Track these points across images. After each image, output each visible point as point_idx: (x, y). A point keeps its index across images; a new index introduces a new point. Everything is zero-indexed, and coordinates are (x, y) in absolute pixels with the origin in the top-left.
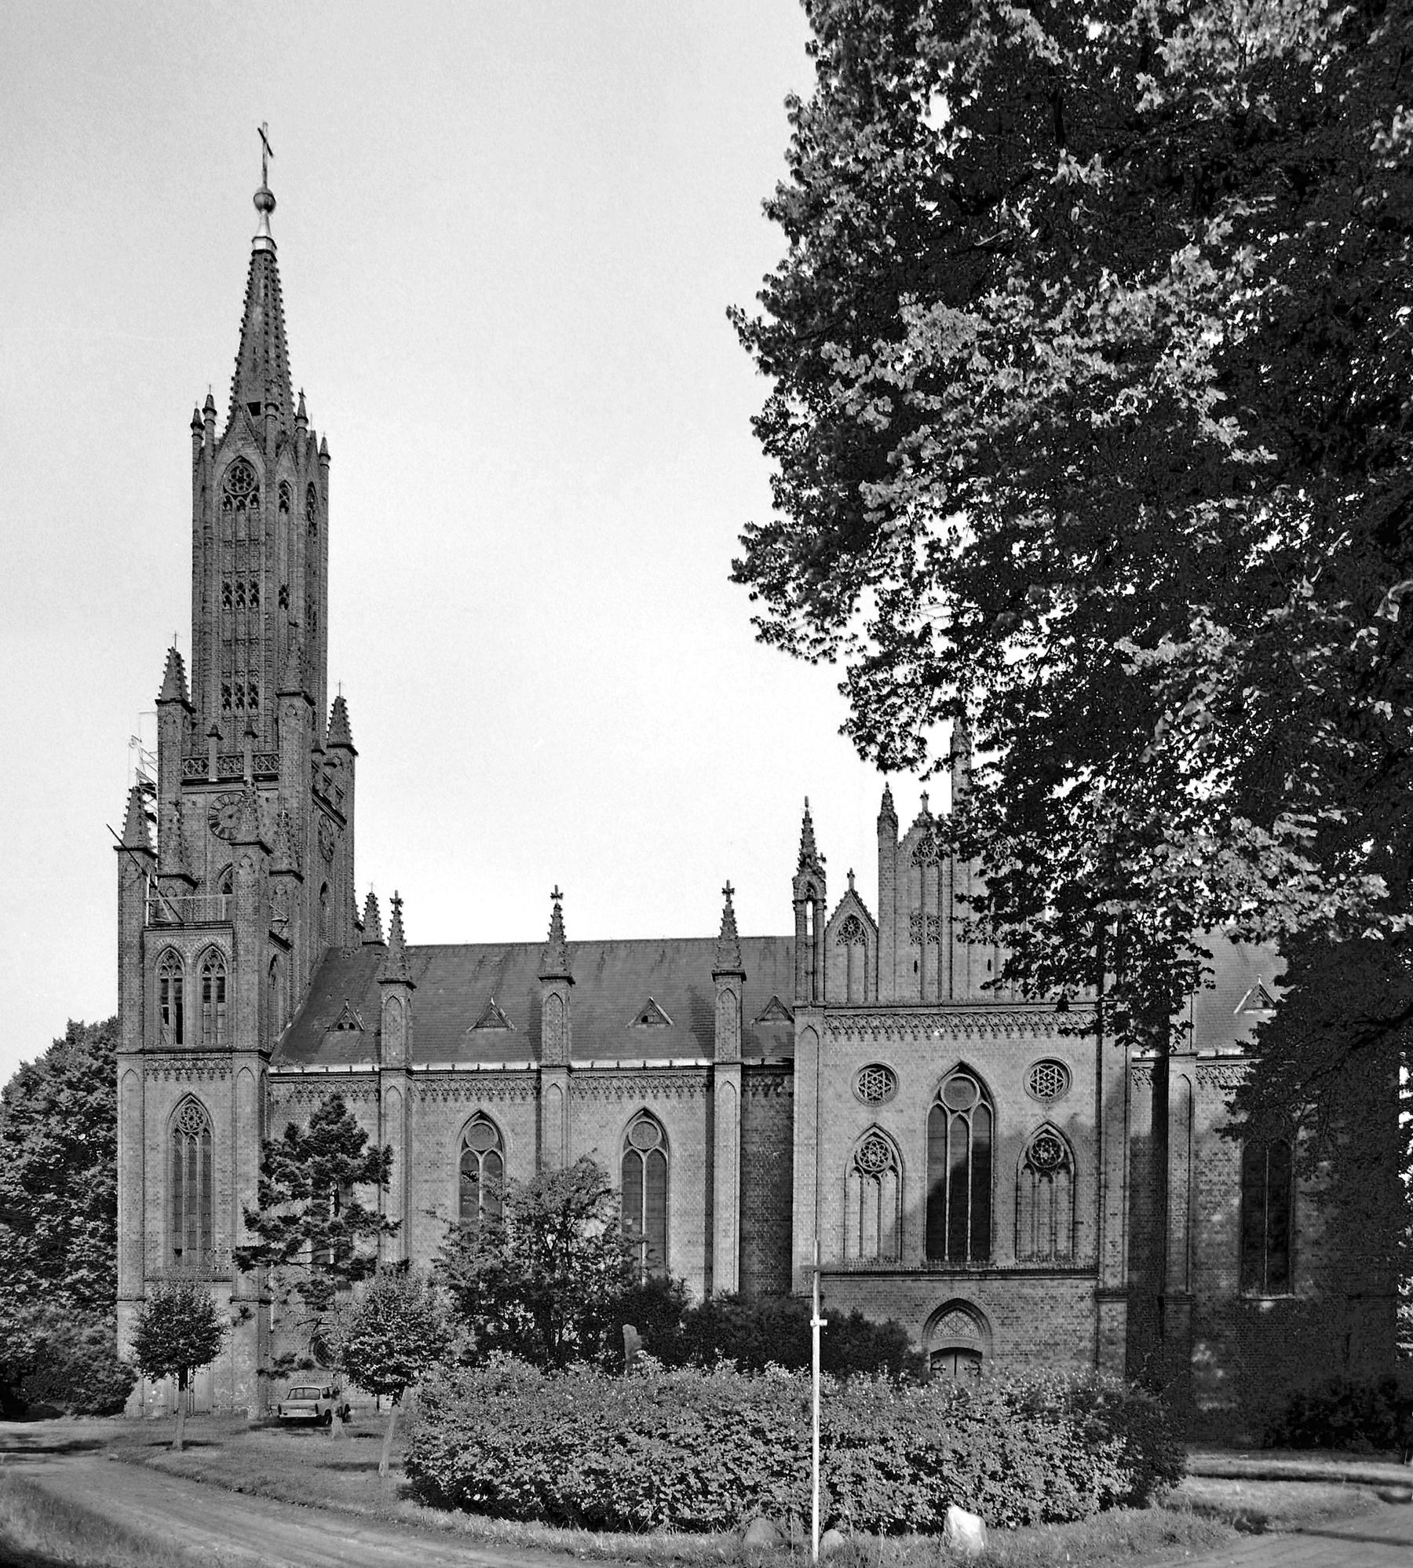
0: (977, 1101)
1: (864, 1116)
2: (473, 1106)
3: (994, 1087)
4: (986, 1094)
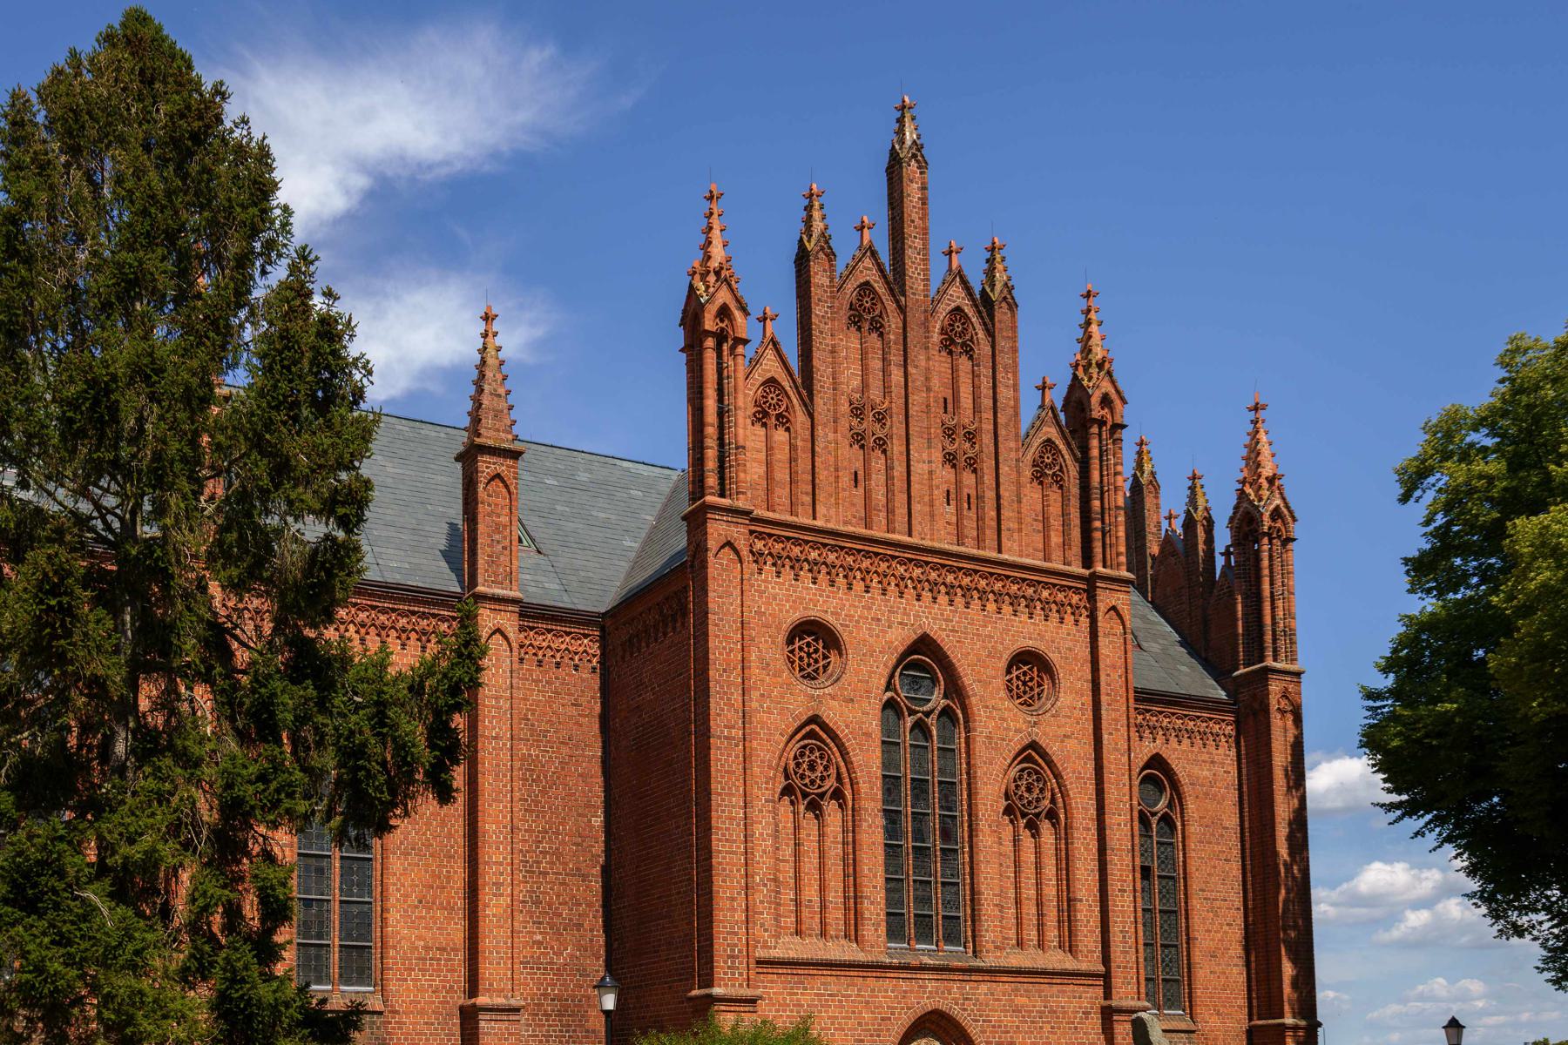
0: (937, 700)
1: (799, 700)
3: (968, 679)
4: (955, 689)
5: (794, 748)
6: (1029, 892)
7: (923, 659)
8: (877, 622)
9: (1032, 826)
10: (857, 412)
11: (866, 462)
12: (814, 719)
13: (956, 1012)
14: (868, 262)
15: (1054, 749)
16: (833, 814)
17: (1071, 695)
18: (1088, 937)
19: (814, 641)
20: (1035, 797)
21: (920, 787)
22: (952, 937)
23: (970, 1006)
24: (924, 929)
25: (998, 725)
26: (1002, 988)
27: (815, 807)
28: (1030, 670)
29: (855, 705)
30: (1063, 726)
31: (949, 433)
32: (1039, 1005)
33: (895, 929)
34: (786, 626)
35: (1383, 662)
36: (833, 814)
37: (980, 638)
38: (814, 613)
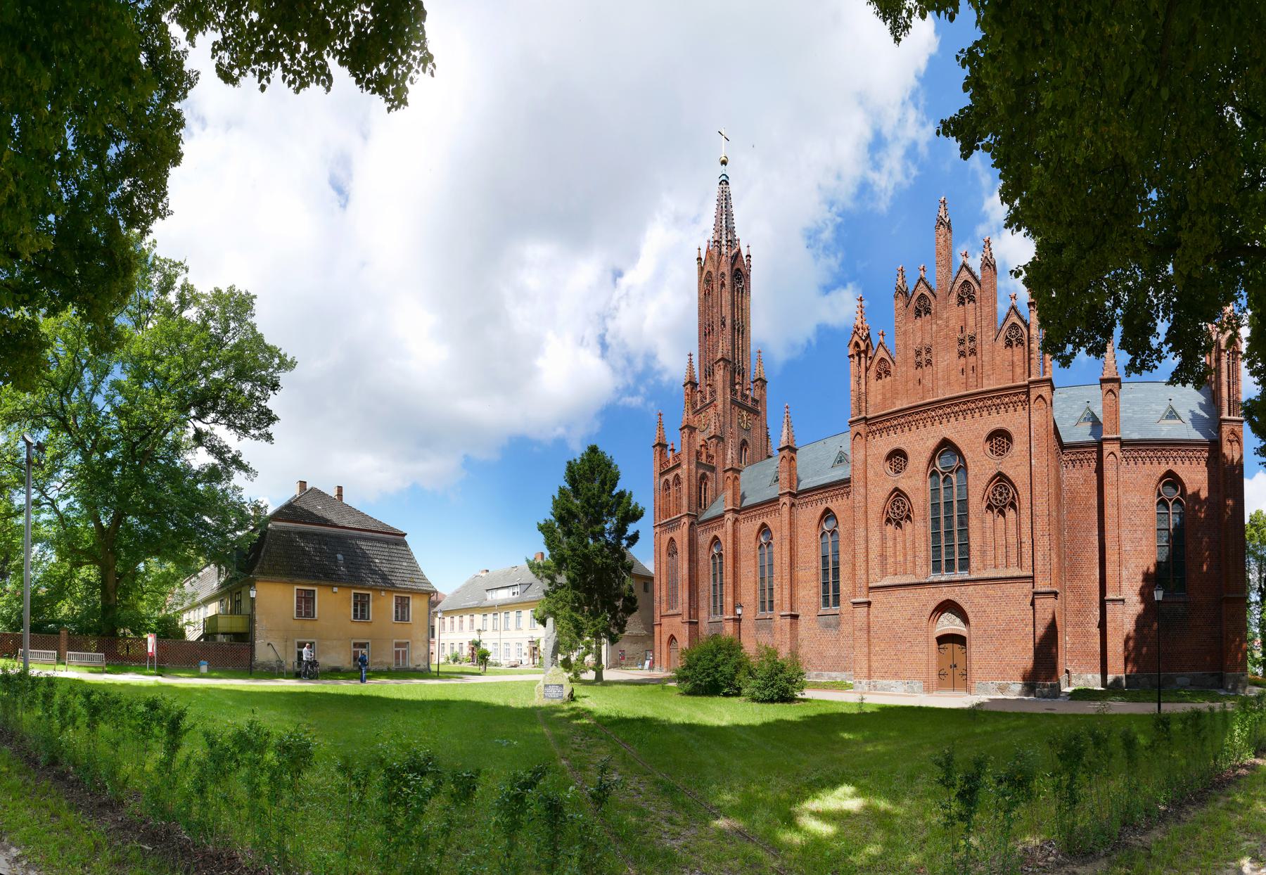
2: (824, 506)
5: (991, 488)
6: (1012, 540)
7: (946, 446)
8: (920, 442)
9: (1002, 513)
10: (918, 353)
11: (206, 602)
12: (896, 489)
13: (957, 600)
14: (922, 285)
15: (1010, 473)
16: (1010, 514)
17: (1018, 446)
18: (1027, 561)
19: (897, 457)
20: (1003, 495)
21: (949, 504)
22: (961, 568)
23: (964, 597)
24: (950, 566)
25: (982, 465)
26: (980, 588)
27: (1002, 513)
28: (1000, 438)
29: (915, 482)
30: (1013, 465)
31: (961, 342)
32: (1000, 593)
33: (936, 568)
34: (985, 435)
35: (542, 523)
36: (1010, 514)
37: (968, 432)
38: (896, 446)
